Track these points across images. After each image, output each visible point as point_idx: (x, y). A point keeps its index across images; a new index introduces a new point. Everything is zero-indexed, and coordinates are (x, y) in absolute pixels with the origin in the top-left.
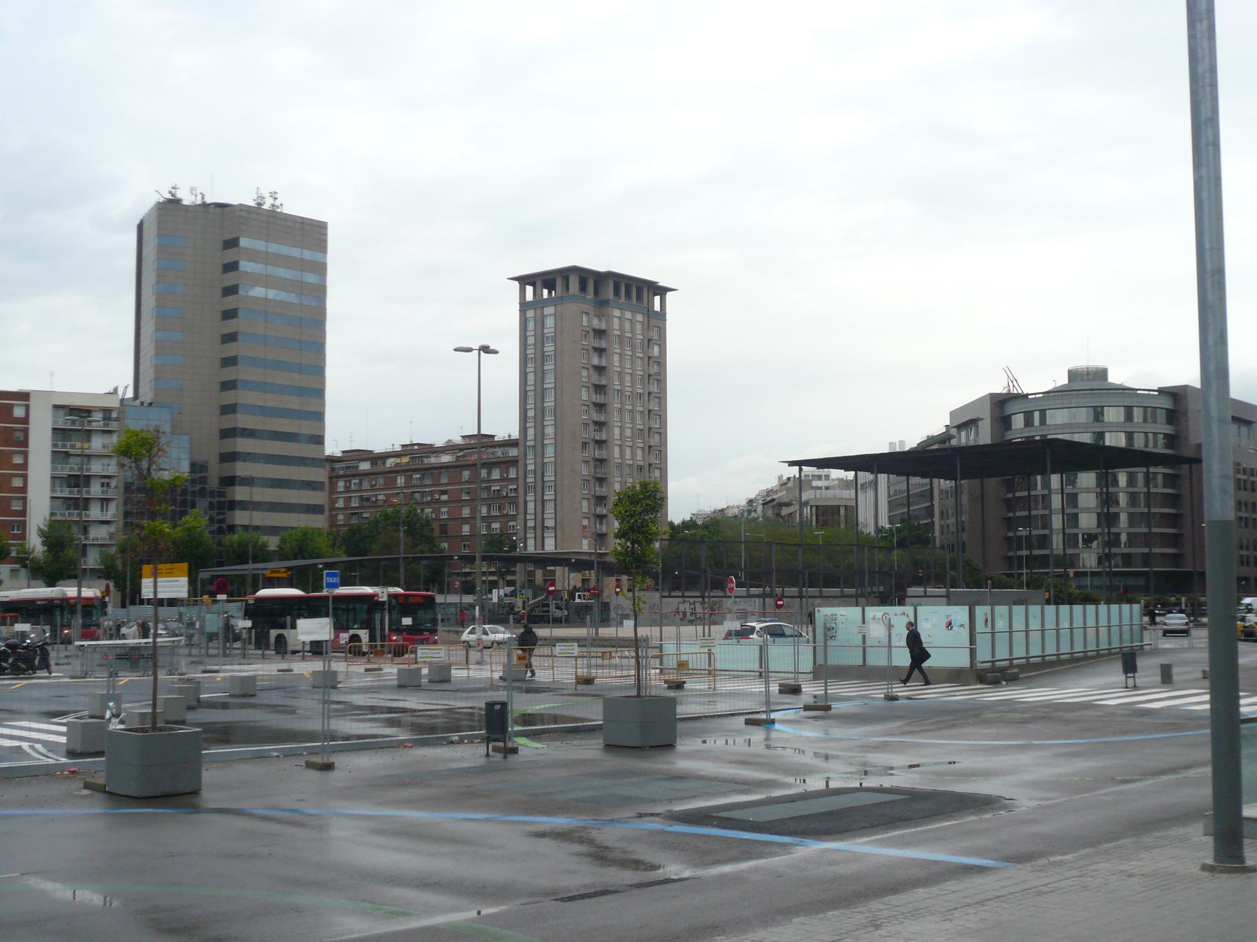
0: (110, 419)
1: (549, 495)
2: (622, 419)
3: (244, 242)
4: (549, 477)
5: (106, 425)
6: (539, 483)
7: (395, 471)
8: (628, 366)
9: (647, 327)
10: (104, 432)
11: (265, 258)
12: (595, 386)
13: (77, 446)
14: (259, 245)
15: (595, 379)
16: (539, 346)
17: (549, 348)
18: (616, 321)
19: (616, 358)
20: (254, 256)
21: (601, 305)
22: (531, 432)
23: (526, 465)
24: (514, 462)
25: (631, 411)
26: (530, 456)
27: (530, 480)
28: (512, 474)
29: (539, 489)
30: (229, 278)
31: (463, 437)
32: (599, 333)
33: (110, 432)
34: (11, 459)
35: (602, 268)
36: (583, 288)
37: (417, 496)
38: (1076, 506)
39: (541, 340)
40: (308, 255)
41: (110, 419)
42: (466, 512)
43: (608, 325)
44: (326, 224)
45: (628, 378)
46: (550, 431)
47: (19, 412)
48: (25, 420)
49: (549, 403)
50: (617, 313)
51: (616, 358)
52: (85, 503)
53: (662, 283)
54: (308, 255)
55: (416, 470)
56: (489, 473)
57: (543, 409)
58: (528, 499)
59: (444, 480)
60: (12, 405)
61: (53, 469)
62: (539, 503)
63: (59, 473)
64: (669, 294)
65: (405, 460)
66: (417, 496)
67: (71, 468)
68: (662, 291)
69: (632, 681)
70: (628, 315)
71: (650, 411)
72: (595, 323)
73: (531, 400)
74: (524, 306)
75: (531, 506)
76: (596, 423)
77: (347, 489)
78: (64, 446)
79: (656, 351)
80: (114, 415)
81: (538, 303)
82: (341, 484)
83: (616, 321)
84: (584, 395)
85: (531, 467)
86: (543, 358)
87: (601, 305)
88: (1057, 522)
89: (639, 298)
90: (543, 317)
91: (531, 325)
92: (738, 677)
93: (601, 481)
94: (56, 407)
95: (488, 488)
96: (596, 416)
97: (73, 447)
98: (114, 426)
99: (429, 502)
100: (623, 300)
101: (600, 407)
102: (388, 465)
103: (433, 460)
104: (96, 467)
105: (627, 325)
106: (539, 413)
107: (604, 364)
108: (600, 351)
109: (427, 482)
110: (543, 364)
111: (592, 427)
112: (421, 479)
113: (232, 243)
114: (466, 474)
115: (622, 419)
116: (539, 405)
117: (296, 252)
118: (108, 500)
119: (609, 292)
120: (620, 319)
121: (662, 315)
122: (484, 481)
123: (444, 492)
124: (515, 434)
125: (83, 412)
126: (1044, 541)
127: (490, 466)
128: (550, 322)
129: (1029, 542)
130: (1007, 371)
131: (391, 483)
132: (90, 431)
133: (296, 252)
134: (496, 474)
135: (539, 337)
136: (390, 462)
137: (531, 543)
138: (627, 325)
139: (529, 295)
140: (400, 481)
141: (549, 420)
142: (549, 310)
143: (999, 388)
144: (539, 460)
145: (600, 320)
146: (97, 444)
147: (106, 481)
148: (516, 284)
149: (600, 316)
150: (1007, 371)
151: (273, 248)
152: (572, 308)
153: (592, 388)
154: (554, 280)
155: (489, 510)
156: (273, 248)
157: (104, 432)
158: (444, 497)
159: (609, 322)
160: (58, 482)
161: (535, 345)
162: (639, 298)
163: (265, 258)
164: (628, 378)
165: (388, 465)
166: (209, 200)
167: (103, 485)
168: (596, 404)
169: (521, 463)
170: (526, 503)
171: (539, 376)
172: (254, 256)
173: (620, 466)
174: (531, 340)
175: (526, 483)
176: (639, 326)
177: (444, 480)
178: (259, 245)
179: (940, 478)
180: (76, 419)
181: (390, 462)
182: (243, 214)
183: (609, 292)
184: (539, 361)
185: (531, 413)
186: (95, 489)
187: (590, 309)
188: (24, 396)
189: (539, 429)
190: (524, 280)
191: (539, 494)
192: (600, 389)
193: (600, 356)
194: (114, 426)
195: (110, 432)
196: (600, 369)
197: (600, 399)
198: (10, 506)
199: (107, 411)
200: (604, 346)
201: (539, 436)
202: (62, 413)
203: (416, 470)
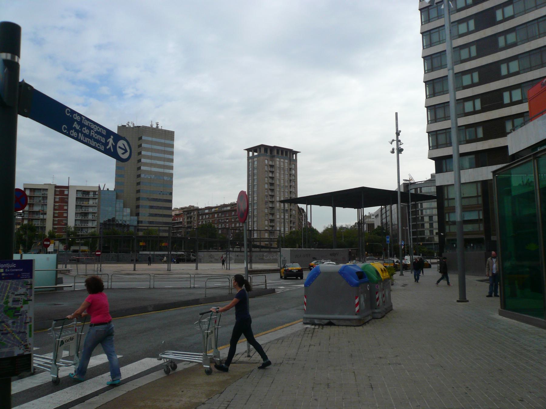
0: (96, 194)
2: (280, 194)
3: (143, 138)
4: (255, 213)
10: (93, 199)
11: (152, 143)
13: (85, 203)
14: (150, 139)
15: (270, 181)
17: (255, 171)
20: (147, 142)
21: (272, 157)
32: (272, 166)
33: (96, 199)
36: (278, 153)
38: (423, 221)
39: (253, 169)
40: (167, 142)
41: (96, 194)
46: (256, 198)
47: (66, 193)
50: (278, 159)
52: (87, 221)
54: (167, 142)
55: (220, 212)
57: (254, 191)
59: (227, 215)
63: (78, 212)
65: (217, 209)
68: (296, 153)
70: (282, 160)
71: (290, 192)
72: (271, 163)
73: (250, 189)
74: (249, 158)
75: (250, 223)
76: (270, 195)
77: (202, 218)
79: (293, 172)
80: (97, 193)
82: (200, 217)
84: (266, 186)
87: (272, 157)
88: (427, 226)
90: (254, 162)
94: (77, 191)
96: (270, 193)
98: (97, 197)
101: (272, 190)
103: (225, 209)
104: (91, 210)
105: (282, 164)
108: (272, 172)
109: (223, 216)
111: (269, 197)
113: (140, 138)
114: (233, 213)
115: (280, 194)
117: (163, 141)
118: (94, 220)
120: (279, 162)
121: (296, 161)
123: (227, 219)
126: (423, 233)
128: (256, 163)
129: (37, 213)
130: (410, 175)
131: (213, 217)
133: (163, 141)
136: (213, 210)
138: (282, 164)
140: (216, 215)
141: (255, 195)
146: (91, 202)
149: (272, 161)
150: (410, 175)
151: (154, 139)
156: (154, 139)
157: (93, 199)
158: (227, 221)
160: (79, 215)
163: (152, 143)
166: (136, 125)
168: (270, 189)
172: (147, 142)
173: (279, 210)
174: (250, 169)
178: (150, 139)
181: (213, 210)
186: (90, 217)
188: (67, 187)
190: (249, 150)
192: (272, 184)
194: (97, 197)
195: (96, 199)
196: (272, 178)
197: (272, 188)
199: (94, 192)
203: (220, 212)
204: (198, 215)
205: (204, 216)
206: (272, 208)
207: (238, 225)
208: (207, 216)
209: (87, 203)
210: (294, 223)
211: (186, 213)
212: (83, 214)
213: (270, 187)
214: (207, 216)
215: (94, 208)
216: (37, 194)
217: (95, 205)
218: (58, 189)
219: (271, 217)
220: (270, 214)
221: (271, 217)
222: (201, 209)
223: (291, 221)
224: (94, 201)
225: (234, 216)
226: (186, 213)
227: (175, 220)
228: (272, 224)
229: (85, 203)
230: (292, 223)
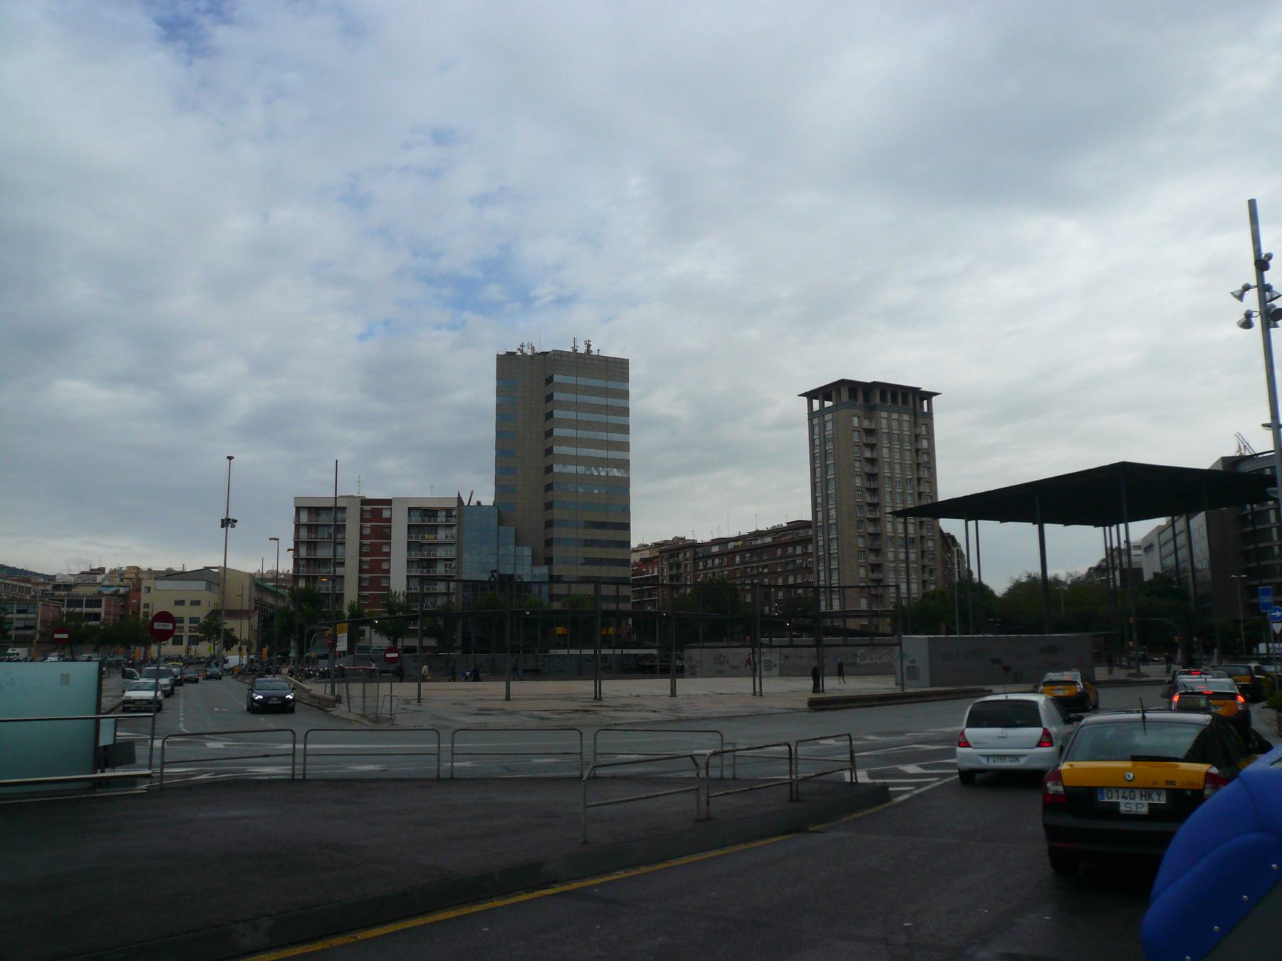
1: (834, 565)
3: (557, 378)
7: (733, 553)
8: (897, 456)
9: (916, 425)
11: (576, 389)
13: (429, 538)
14: (570, 380)
15: (868, 469)
18: (884, 422)
19: (885, 451)
20: (565, 388)
21: (870, 410)
22: (820, 515)
24: (806, 541)
26: (820, 534)
28: (810, 548)
30: (559, 405)
32: (870, 432)
35: (868, 379)
39: (824, 441)
40: (612, 385)
42: (780, 582)
45: (897, 467)
46: (833, 513)
47: (386, 514)
48: (389, 520)
50: (884, 414)
51: (885, 451)
53: (925, 388)
54: (612, 385)
61: (409, 555)
64: (934, 398)
65: (740, 543)
67: (417, 556)
70: (895, 416)
72: (866, 424)
75: (822, 574)
76: (869, 504)
79: (925, 444)
80: (454, 513)
83: (884, 422)
84: (858, 482)
85: (821, 543)
86: (825, 455)
87: (870, 410)
89: (905, 402)
90: (825, 423)
92: (645, 723)
93: (877, 551)
94: (410, 509)
98: (454, 521)
100: (889, 403)
101: (874, 491)
104: (441, 553)
105: (895, 424)
108: (872, 447)
109: (755, 559)
113: (549, 380)
117: (601, 383)
119: (877, 398)
120: (887, 420)
121: (929, 415)
122: (790, 556)
123: (766, 567)
125: (429, 513)
128: (829, 426)
130: (1239, 436)
131: (731, 562)
133: (601, 383)
134: (799, 550)
136: (731, 545)
137: (823, 604)
138: (895, 424)
139: (816, 404)
140: (738, 559)
141: (832, 505)
142: (828, 417)
143: (1232, 452)
146: (442, 535)
149: (870, 419)
150: (1239, 436)
151: (582, 381)
156: (582, 381)
158: (766, 570)
162: (905, 402)
163: (576, 389)
164: (897, 467)
166: (538, 350)
168: (869, 490)
173: (892, 539)
176: (906, 425)
178: (570, 380)
179: (976, 519)
180: (426, 518)
181: (731, 545)
183: (877, 398)
185: (819, 500)
186: (440, 570)
190: (810, 395)
194: (454, 521)
195: (451, 526)
196: (872, 461)
205: (710, 562)
206: (876, 536)
207: (791, 580)
208: (717, 561)
209: (432, 537)
210: (931, 572)
214: (717, 561)
215: (448, 548)
216: (325, 519)
217: (449, 540)
218: (368, 508)
219: (872, 558)
221: (872, 558)
222: (703, 545)
223: (924, 567)
224: (449, 532)
225: (781, 558)
228: (876, 576)
229: (429, 538)
230: (927, 570)
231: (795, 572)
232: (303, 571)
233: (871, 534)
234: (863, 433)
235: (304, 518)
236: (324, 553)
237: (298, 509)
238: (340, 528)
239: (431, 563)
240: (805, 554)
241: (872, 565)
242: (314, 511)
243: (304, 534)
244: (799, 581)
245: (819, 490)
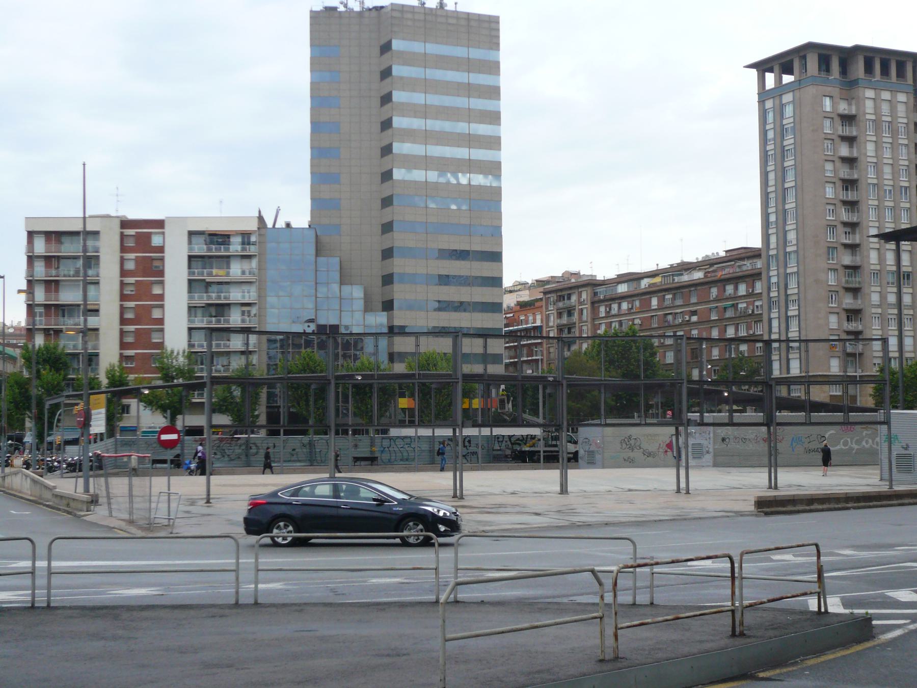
3: (397, 45)
4: (793, 289)
5: (244, 249)
6: (783, 298)
7: (650, 293)
10: (243, 257)
11: (424, 60)
12: (844, 181)
13: (218, 273)
14: (417, 47)
15: (844, 172)
16: (778, 140)
18: (869, 105)
20: (409, 59)
21: (849, 85)
22: (773, 239)
23: (769, 278)
24: (756, 276)
25: (893, 209)
26: (773, 267)
27: (774, 294)
28: (759, 287)
29: (783, 303)
31: (727, 252)
32: (848, 119)
33: (249, 257)
34: (150, 290)
35: (848, 43)
37: (670, 318)
39: (782, 132)
40: (476, 54)
43: (858, 109)
44: (498, 18)
45: (887, 170)
47: (156, 241)
49: (790, 205)
50: (870, 93)
54: (476, 54)
55: (667, 290)
56: (736, 289)
57: (785, 211)
58: (773, 316)
59: (694, 300)
60: (150, 233)
62: (783, 320)
65: (658, 280)
66: (670, 318)
67: (202, 299)
69: (29, 598)
70: (886, 95)
72: (843, 108)
74: (763, 96)
75: (775, 324)
76: (845, 224)
77: (608, 315)
78: (202, 274)
81: (780, 88)
82: (602, 309)
83: (869, 105)
84: (830, 192)
85: (774, 280)
87: (849, 85)
90: (782, 106)
91: (770, 117)
94: (191, 234)
95: (735, 306)
96: (845, 216)
97: (210, 274)
98: (253, 250)
99: (680, 325)
101: (852, 205)
102: (643, 286)
104: (236, 295)
105: (885, 108)
106: (781, 217)
107: (855, 155)
108: (850, 140)
109: (679, 302)
110: (783, 160)
111: (841, 229)
112: (674, 299)
113: (386, 48)
114: (714, 292)
116: (780, 207)
117: (460, 52)
119: (858, 69)
122: (730, 298)
123: (694, 313)
124: (756, 242)
125: (219, 238)
127: (736, 280)
128: (789, 111)
132: (228, 257)
133: (460, 52)
134: (742, 289)
135: (778, 130)
136: (645, 283)
138: (885, 108)
140: (654, 302)
141: (791, 225)
144: (782, 271)
145: (850, 104)
146: (236, 270)
147: (246, 309)
148: (754, 72)
149: (848, 100)
151: (432, 48)
152: (810, 91)
153: (839, 184)
154: (791, 63)
155: (737, 330)
156: (432, 48)
157: (243, 257)
158: (694, 319)
159: (860, 102)
161: (774, 139)
163: (424, 60)
164: (887, 170)
165: (643, 286)
167: (243, 313)
168: (845, 203)
169: (764, 276)
170: (770, 320)
171: (780, 174)
173: (877, 274)
175: (770, 298)
177: (694, 300)
178: (417, 47)
181: (645, 283)
182: (396, 14)
183: (858, 69)
184: (779, 156)
185: (773, 218)
187: (836, 92)
189: (781, 235)
190: (762, 67)
191: (783, 310)
193: (851, 146)
195: (249, 257)
196: (850, 161)
197: (851, 196)
198: (150, 338)
200: (854, 134)
201: (781, 242)
202: (201, 239)
203: (667, 290)
204: (595, 304)
205: (615, 306)
206: (854, 269)
207: (730, 333)
211: (553, 297)
212: (213, 311)
213: (842, 195)
215: (245, 288)
216: (69, 248)
217: (247, 277)
218: (132, 232)
219: (848, 301)
220: (847, 290)
221: (848, 301)
222: (603, 283)
225: (717, 300)
226: (553, 297)
227: (521, 322)
229: (218, 273)
231: (735, 321)
232: (41, 322)
233: (847, 267)
234: (841, 271)
235: (40, 247)
236: (69, 296)
237: (31, 235)
238: (91, 261)
239: (221, 309)
240: (750, 295)
241: (847, 311)
242: (55, 237)
243: (40, 269)
244: (743, 333)
245: (772, 203)
